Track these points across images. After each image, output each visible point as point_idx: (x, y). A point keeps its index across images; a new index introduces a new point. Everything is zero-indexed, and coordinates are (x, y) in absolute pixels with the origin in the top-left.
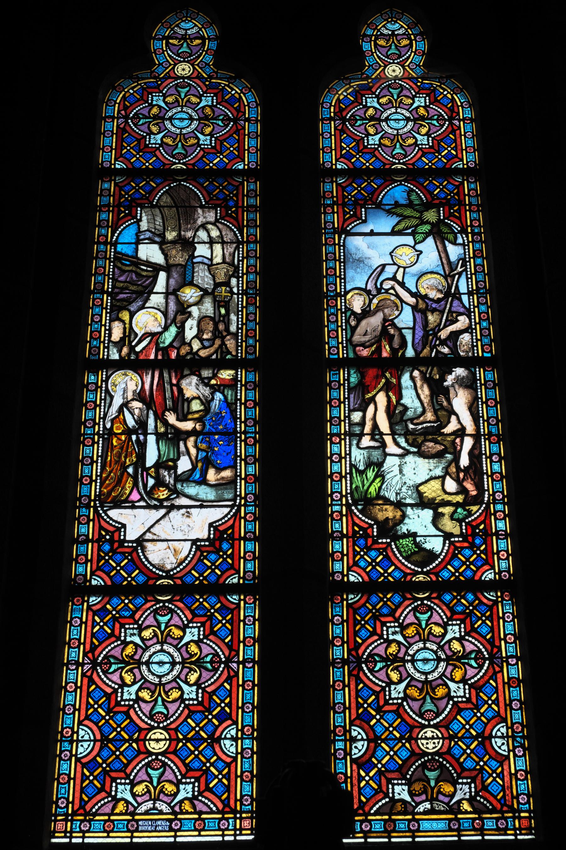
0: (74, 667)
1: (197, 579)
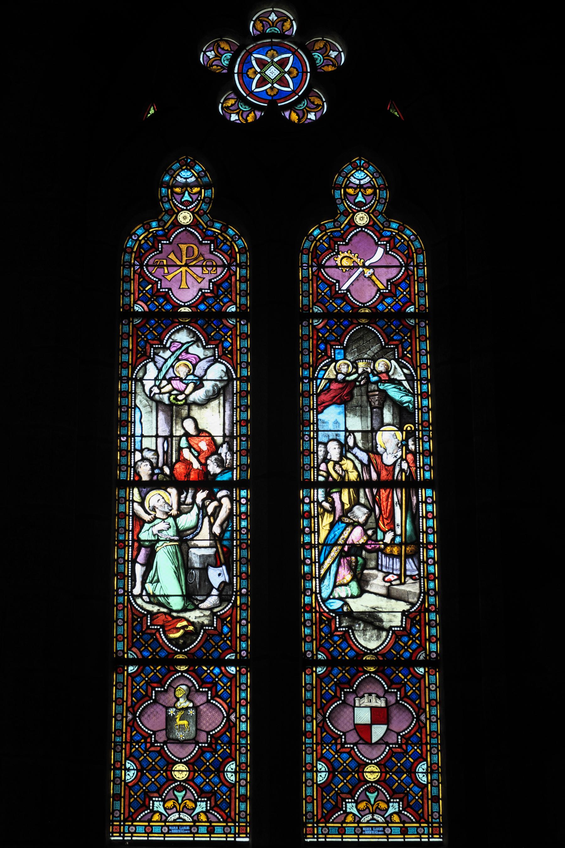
1: (396, 656)
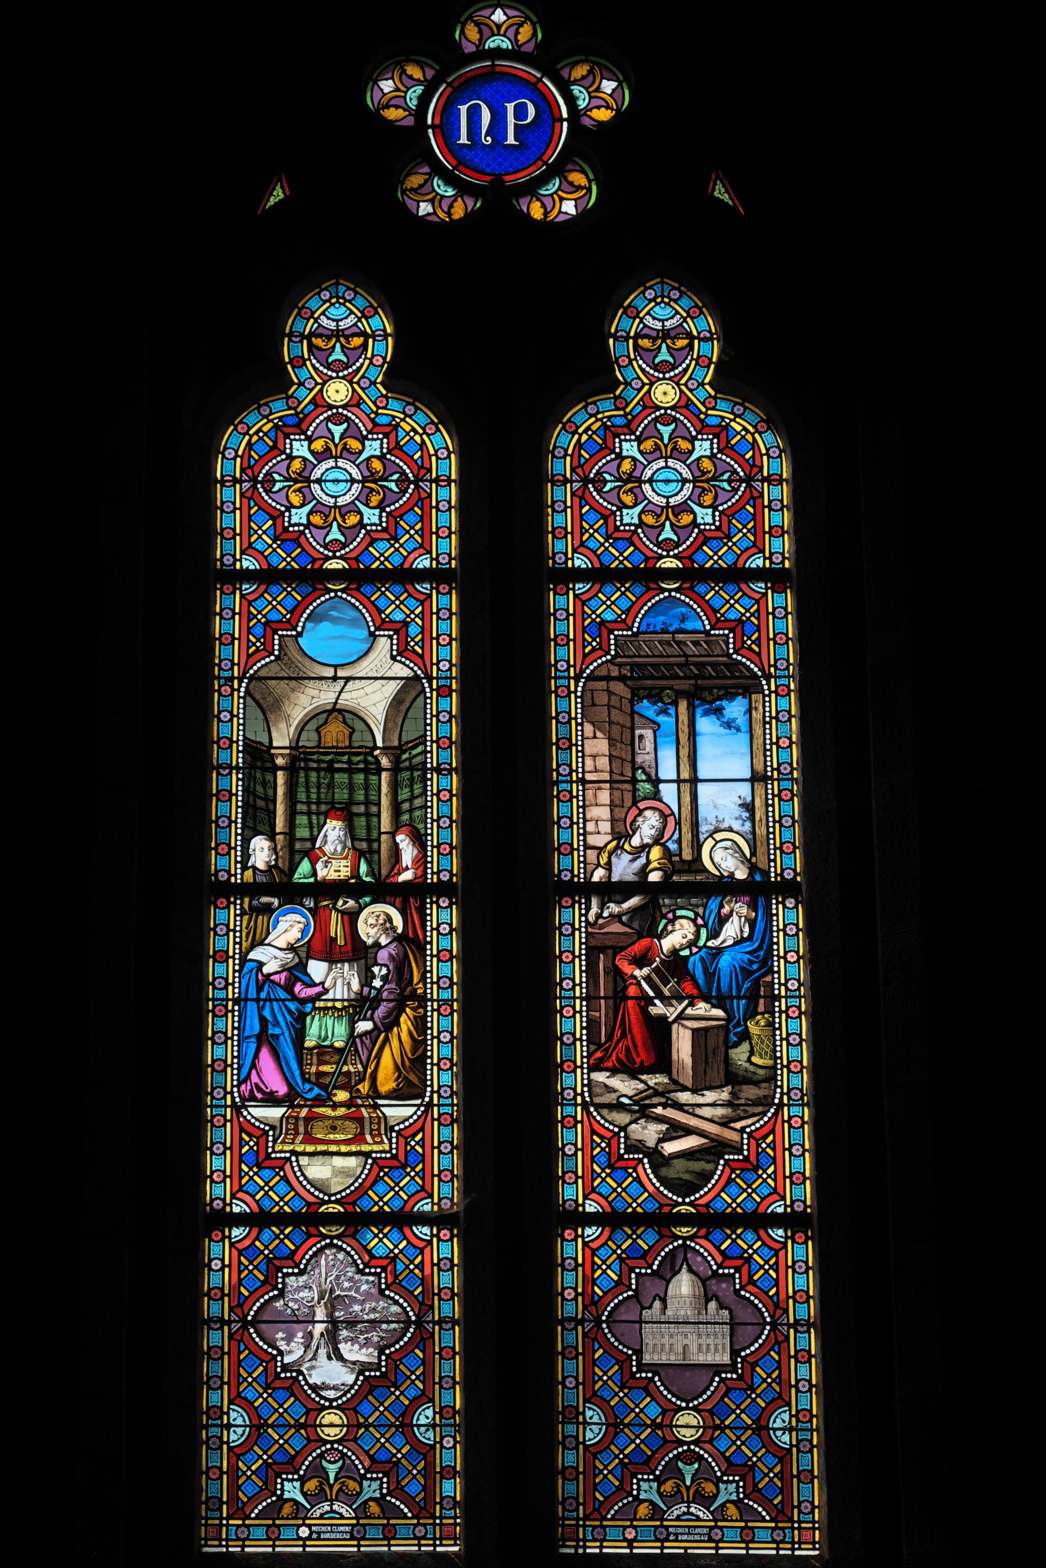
0: (450, 1325)
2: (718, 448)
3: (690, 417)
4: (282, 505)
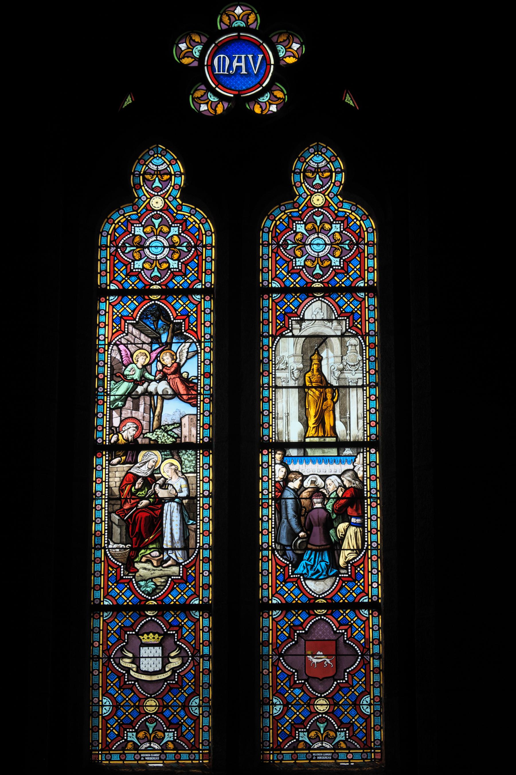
0: (208, 658)
2: (343, 228)
3: (169, 214)
4: (130, 259)
